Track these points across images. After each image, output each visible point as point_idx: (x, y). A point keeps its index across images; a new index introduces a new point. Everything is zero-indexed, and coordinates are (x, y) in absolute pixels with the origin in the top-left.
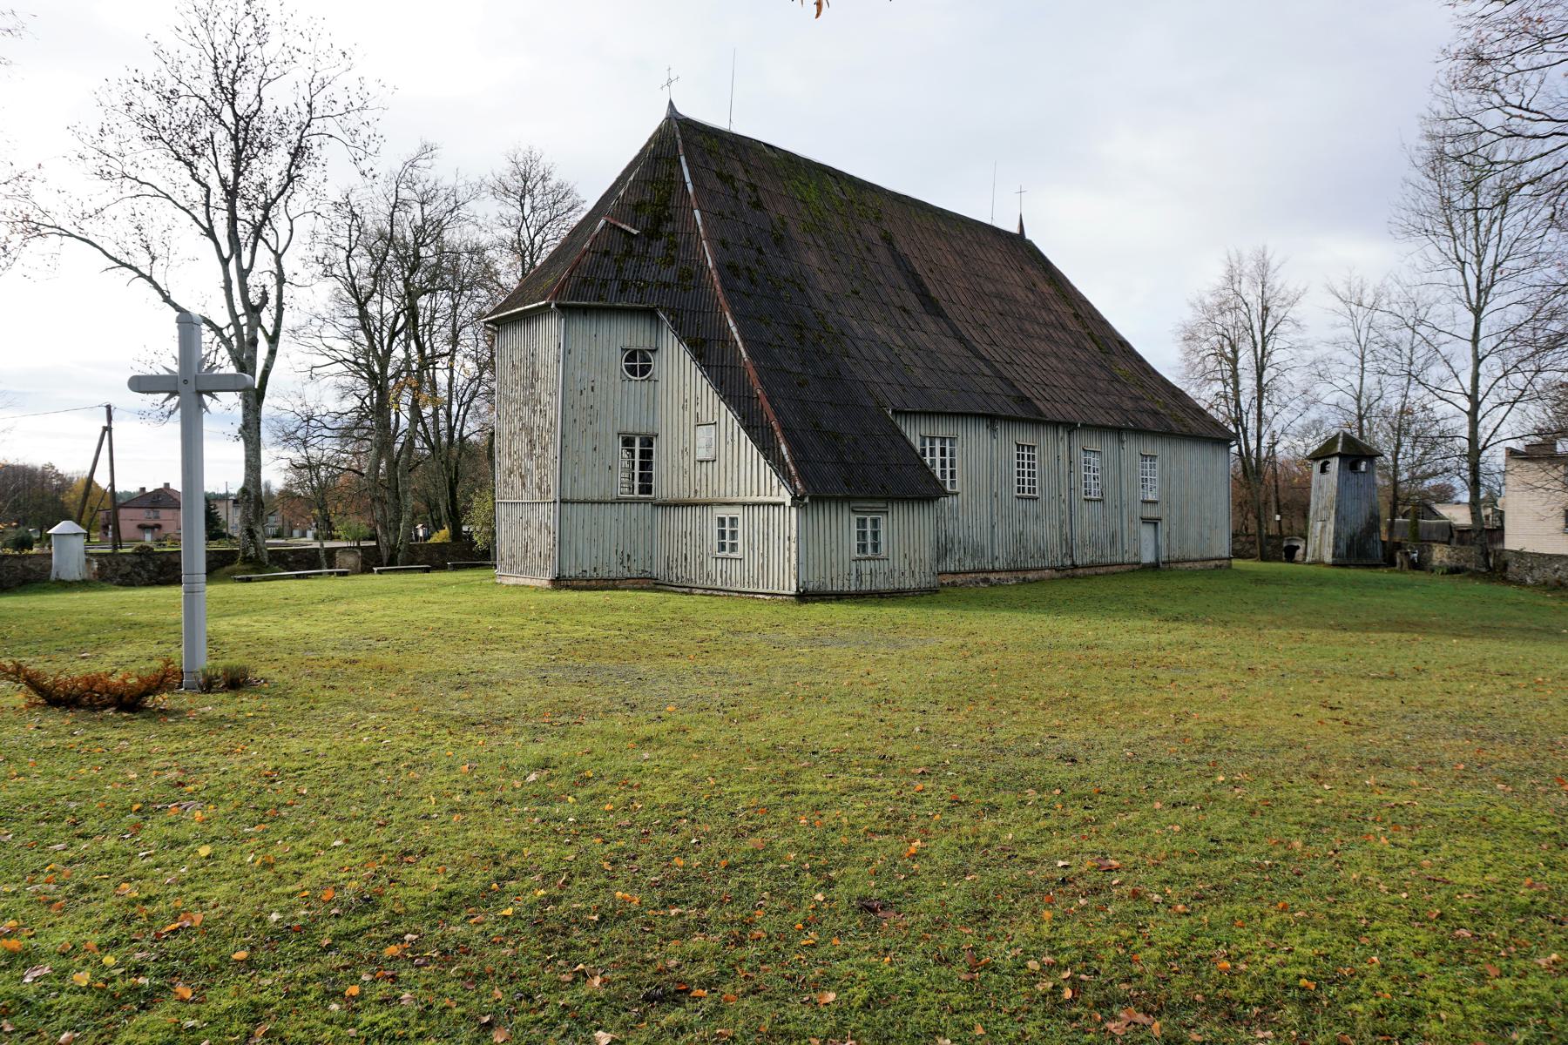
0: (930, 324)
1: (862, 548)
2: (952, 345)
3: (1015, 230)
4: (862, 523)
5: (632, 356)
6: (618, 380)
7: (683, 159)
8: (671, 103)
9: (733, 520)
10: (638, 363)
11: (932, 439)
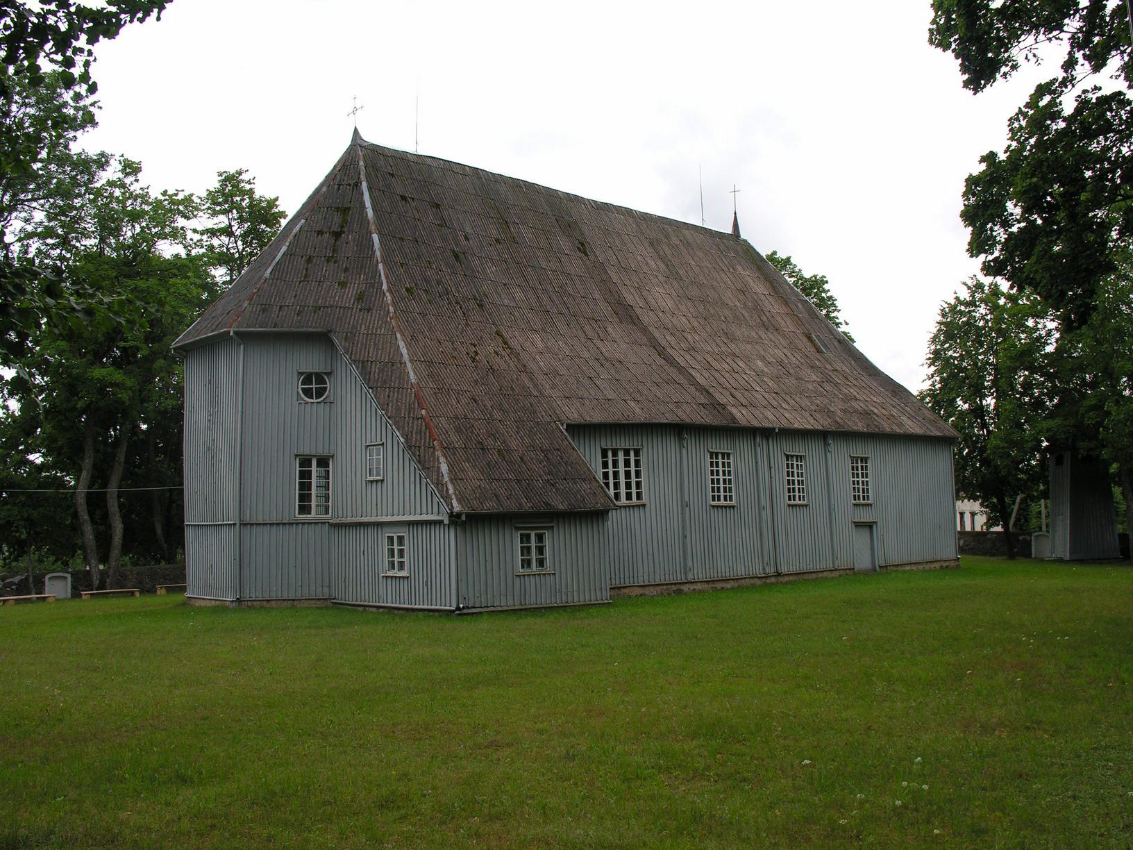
0: (615, 330)
1: (527, 563)
2: (646, 352)
3: (729, 231)
5: (308, 379)
7: (364, 185)
8: (356, 130)
9: (401, 539)
10: (314, 385)
11: (615, 453)
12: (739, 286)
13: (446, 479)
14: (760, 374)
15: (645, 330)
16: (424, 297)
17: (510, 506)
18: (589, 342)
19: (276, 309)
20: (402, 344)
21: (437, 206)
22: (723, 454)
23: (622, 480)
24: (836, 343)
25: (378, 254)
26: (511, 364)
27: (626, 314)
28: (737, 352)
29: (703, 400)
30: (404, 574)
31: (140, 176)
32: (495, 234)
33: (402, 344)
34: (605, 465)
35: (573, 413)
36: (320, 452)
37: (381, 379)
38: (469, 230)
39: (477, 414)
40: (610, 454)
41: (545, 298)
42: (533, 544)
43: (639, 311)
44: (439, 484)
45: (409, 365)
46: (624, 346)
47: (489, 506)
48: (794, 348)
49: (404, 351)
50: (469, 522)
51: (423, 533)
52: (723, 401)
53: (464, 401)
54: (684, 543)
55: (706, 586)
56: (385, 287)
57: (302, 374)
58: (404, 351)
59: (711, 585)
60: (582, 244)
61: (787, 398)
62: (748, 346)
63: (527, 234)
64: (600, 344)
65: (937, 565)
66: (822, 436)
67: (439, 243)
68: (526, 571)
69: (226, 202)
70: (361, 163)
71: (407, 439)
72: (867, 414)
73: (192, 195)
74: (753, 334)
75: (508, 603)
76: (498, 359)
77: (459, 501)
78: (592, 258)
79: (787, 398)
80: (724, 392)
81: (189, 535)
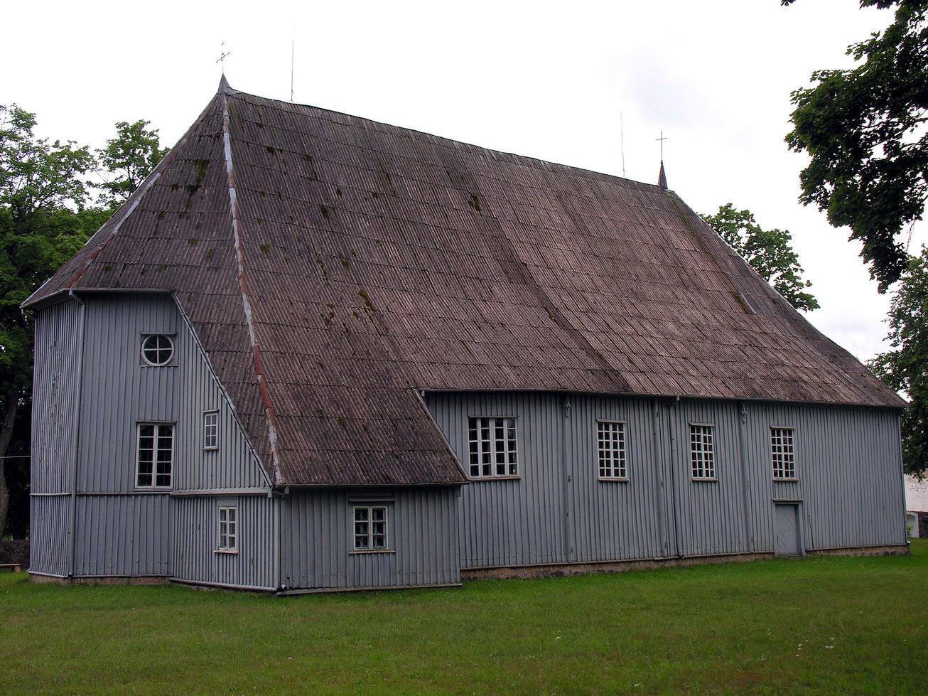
0: (501, 291)
3: (654, 181)
4: (361, 514)
5: (152, 341)
6: (138, 367)
7: (226, 136)
8: (223, 78)
9: (232, 512)
10: (158, 348)
11: (485, 422)
12: (659, 242)
13: (273, 449)
14: (668, 337)
15: (538, 290)
16: (281, 254)
17: (344, 479)
18: (469, 304)
19: (120, 267)
20: (246, 305)
21: (309, 158)
22: (614, 425)
23: (493, 452)
24: (769, 303)
25: (233, 209)
26: (372, 326)
27: (518, 273)
28: (646, 313)
29: (593, 366)
30: (234, 550)
31: (34, 129)
32: (372, 187)
33: (246, 305)
34: (473, 435)
35: (435, 379)
36: (162, 419)
37: (222, 343)
38: (342, 183)
39: (323, 380)
40: (479, 424)
41: (423, 257)
42: (370, 521)
43: (532, 269)
44: (265, 455)
45: (251, 327)
46: (509, 307)
47: (319, 479)
48: (716, 308)
49: (248, 312)
50: (295, 495)
51: (250, 507)
52: (616, 365)
53: (309, 365)
54: (566, 522)
55: (590, 569)
56: (237, 245)
57: (146, 336)
58: (248, 312)
59: (597, 568)
60: (475, 198)
61: (697, 363)
62: (661, 308)
63: (411, 188)
64: (481, 305)
65: (881, 551)
66: (737, 405)
67: (306, 198)
68: (362, 549)
69: (125, 154)
70: (226, 113)
71: (238, 407)
72: (794, 381)
73: (86, 147)
74: (669, 293)
75: (340, 584)
76: (356, 321)
77: (283, 473)
78: (485, 212)
79: (697, 363)
80: (621, 357)
81: (35, 506)
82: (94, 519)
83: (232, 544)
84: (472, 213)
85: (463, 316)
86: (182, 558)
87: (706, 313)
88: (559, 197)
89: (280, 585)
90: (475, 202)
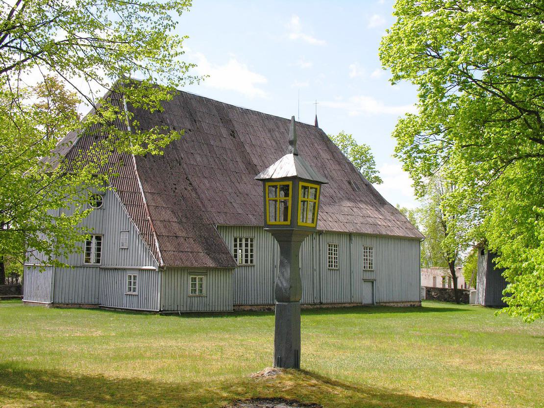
4: (194, 280)
9: (135, 277)
44: (155, 253)
60: (233, 132)
61: (332, 215)
64: (237, 185)
82: (64, 278)
83: (134, 291)
84: (232, 140)
85: (230, 190)
86: (106, 296)
87: (335, 190)
88: (269, 131)
89: (160, 309)
90: (233, 134)
